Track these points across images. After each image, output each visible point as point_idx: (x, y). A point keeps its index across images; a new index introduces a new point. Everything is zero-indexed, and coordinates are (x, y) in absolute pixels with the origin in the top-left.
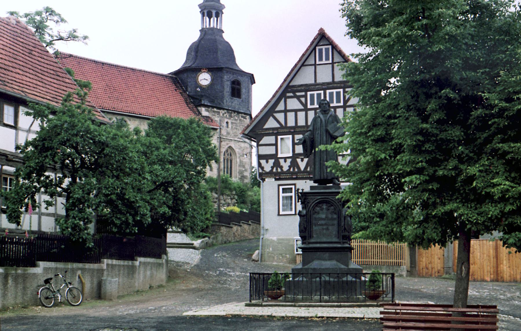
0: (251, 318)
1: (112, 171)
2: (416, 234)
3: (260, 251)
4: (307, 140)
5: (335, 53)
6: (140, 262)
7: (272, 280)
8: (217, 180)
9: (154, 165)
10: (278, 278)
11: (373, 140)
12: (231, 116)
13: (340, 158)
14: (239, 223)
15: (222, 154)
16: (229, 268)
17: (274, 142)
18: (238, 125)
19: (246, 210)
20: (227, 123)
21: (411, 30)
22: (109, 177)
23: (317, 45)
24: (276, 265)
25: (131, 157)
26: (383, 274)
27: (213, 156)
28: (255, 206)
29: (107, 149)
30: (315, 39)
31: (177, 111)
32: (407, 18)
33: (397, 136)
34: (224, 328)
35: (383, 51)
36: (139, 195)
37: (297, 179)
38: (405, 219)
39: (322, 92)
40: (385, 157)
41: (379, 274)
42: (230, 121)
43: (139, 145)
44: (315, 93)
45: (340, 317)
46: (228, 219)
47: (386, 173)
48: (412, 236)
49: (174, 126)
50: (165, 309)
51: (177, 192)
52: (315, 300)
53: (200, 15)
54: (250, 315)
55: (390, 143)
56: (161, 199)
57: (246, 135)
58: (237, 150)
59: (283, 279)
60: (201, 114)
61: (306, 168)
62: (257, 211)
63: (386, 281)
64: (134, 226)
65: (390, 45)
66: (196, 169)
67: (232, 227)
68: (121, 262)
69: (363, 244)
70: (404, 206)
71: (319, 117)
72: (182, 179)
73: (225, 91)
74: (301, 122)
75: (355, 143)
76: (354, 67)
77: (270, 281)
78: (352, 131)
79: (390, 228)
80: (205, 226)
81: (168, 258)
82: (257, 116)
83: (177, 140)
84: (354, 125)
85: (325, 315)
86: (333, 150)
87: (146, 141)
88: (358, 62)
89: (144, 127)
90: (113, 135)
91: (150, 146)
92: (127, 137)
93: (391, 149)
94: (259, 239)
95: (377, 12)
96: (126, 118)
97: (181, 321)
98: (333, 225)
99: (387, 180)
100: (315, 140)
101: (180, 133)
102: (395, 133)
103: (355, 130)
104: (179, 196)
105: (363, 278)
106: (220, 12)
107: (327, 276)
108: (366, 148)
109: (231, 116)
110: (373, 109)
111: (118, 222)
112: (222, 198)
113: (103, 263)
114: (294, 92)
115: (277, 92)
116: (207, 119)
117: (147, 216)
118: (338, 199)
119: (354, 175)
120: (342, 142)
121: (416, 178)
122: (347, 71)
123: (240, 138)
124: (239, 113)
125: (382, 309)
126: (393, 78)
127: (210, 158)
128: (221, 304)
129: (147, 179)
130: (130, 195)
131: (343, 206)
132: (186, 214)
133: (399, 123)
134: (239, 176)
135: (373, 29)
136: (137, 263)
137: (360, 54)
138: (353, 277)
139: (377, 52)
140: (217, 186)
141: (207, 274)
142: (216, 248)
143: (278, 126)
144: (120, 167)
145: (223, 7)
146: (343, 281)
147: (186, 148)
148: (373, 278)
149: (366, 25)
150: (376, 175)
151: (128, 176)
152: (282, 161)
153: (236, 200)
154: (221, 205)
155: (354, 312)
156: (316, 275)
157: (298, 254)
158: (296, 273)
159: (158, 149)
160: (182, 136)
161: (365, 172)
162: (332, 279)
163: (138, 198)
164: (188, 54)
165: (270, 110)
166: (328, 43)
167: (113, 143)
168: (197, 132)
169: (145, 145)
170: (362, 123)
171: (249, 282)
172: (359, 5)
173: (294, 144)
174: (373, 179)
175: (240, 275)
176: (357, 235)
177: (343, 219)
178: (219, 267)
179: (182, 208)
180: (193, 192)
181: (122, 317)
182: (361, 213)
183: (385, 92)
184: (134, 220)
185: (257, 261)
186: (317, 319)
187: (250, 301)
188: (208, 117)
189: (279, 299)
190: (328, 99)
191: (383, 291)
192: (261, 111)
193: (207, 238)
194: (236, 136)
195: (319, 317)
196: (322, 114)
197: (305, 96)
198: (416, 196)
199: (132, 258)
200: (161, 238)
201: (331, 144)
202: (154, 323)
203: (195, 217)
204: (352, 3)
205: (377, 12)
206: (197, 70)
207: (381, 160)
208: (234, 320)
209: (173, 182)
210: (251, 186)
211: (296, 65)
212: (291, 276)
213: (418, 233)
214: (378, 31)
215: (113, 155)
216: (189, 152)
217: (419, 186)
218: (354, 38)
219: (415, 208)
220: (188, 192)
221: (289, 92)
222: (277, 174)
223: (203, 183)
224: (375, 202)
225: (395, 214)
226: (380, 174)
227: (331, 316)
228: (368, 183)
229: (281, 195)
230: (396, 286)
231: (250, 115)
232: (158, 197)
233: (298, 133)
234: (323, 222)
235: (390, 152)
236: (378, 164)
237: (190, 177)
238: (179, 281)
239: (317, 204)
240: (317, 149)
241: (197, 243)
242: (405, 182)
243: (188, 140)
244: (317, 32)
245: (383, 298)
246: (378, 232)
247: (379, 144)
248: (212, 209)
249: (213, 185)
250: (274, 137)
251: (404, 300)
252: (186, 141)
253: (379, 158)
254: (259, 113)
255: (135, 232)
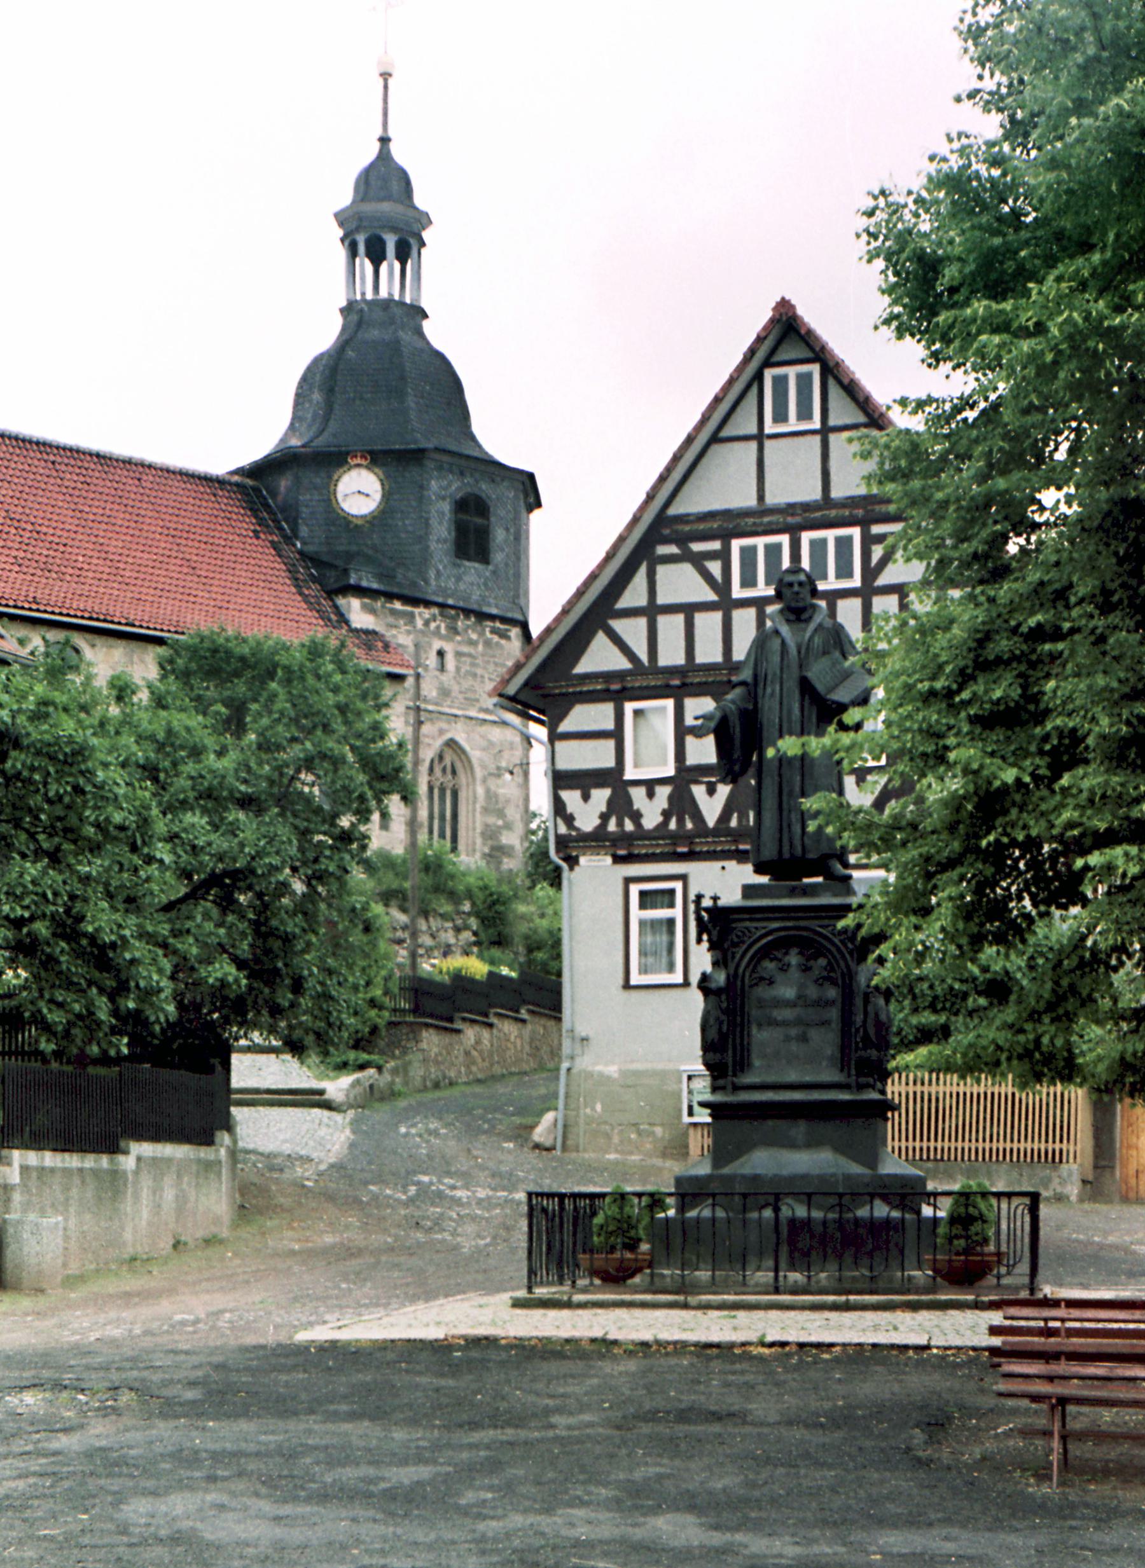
0: (534, 1347)
1: (32, 836)
2: (1122, 1059)
3: (560, 1116)
4: (731, 718)
5: (834, 391)
6: (139, 1159)
7: (607, 1217)
8: (404, 861)
9: (185, 810)
10: (627, 1209)
11: (973, 720)
12: (453, 630)
13: (849, 781)
14: (486, 1015)
15: (424, 768)
16: (449, 1174)
17: (610, 725)
18: (479, 661)
19: (511, 969)
20: (441, 654)
21: (1119, 309)
22: (24, 856)
23: (767, 363)
24: (617, 1163)
25: (104, 782)
26: (999, 1195)
27: (397, 777)
28: (540, 955)
29: (13, 754)
30: (760, 340)
31: (264, 611)
32: (1105, 263)
33: (1064, 703)
34: (443, 1382)
35: (1018, 385)
36: (132, 920)
37: (692, 856)
38: (1083, 1005)
39: (784, 539)
40: (1018, 780)
41: (985, 1195)
42: (448, 648)
43: (128, 740)
44: (760, 542)
45: (844, 1345)
46: (441, 1004)
47: (1021, 838)
48: (1106, 1063)
49: (253, 667)
50: (230, 1322)
51: (266, 906)
52: (757, 1285)
54: (530, 1339)
55: (1038, 730)
56: (211, 934)
57: (513, 699)
58: (475, 755)
59: (646, 1212)
60: (347, 622)
61: (725, 817)
62: (548, 973)
63: (1009, 1219)
64: (114, 1031)
65: (1044, 365)
66: (333, 824)
67: (458, 1031)
68: (73, 1161)
69: (926, 1089)
70: (1082, 958)
71: (777, 632)
72: (284, 862)
73: (433, 538)
74: (709, 652)
75: (907, 730)
76: (907, 447)
77: (599, 1220)
78: (897, 684)
79: (1031, 1037)
80: (367, 1030)
81: (235, 1142)
82: (548, 631)
83: (265, 721)
84: (907, 663)
85: (793, 1336)
86: (828, 754)
87: (155, 726)
88: (921, 428)
89: (144, 669)
90: (38, 704)
91: (167, 743)
92: (84, 708)
93: (1041, 753)
94: (558, 1069)
95: (997, 241)
96: (78, 640)
97: (290, 1361)
98: (825, 1023)
99: (1022, 865)
100: (761, 719)
101: (276, 695)
102: (1055, 691)
103: (911, 681)
104: (274, 923)
105: (927, 1211)
106: (412, 241)
107: (801, 1202)
108: (947, 748)
109: (453, 630)
110: (977, 605)
111: (56, 1017)
112: (424, 927)
113: (9, 1164)
114: (682, 540)
115: (621, 539)
116: (368, 638)
117: (163, 996)
118: (845, 930)
119: (904, 844)
120: (858, 727)
121: (1126, 854)
122: (882, 463)
123: (486, 711)
124: (482, 616)
125: (996, 1318)
126: (1052, 489)
127: (384, 786)
128: (427, 1300)
129: (161, 861)
130: (102, 919)
131: (862, 958)
132: (298, 986)
133: (1073, 652)
134: (482, 847)
135: (980, 307)
136: (128, 1162)
137: (930, 400)
138: (894, 1207)
139: (995, 389)
140: (407, 885)
141: (375, 1197)
142: (402, 1103)
143: (624, 664)
144: (60, 819)
145: (424, 221)
146: (857, 1220)
147: (297, 747)
148: (962, 1210)
149: (953, 290)
150: (984, 843)
151: (91, 851)
152: (638, 794)
153: (475, 934)
154: (421, 951)
155: (896, 1328)
156: (762, 1200)
157: (695, 1125)
158: (690, 1192)
159: (196, 752)
160: (282, 703)
161: (944, 836)
162: (817, 1214)
163: (127, 932)
164: (301, 398)
165: (596, 610)
166: (811, 355)
167: (37, 733)
168: (336, 690)
169: (152, 738)
170: (937, 655)
171: (524, 1224)
172: (927, 211)
173: (681, 732)
174: (970, 858)
175: (489, 1198)
176: (909, 1058)
177: (859, 1002)
178: (415, 1173)
179: (286, 965)
180: (323, 906)
181: (80, 1350)
182: (920, 979)
183: (1022, 541)
184: (115, 1013)
185: (548, 1149)
186: (766, 1351)
187: (530, 1289)
188: (374, 633)
189: (629, 1282)
190: (805, 564)
191: (999, 1254)
192: (565, 612)
193: (372, 1071)
194: (472, 701)
195: (772, 1345)
196: (788, 621)
197: (724, 556)
198: (1129, 918)
199: (112, 1147)
200: (210, 1070)
201: (820, 733)
202: (195, 1367)
203: (331, 998)
204: (905, 206)
205: (997, 241)
206: (330, 461)
207: (1005, 789)
208: (475, 1354)
209: (253, 872)
210: (528, 883)
211: (689, 440)
212: (670, 1201)
213: (1130, 1049)
214: (1001, 311)
215: (37, 777)
216: (308, 764)
217: (1137, 884)
218: (908, 338)
219: (1122, 964)
220: (305, 908)
221: (666, 541)
222: (624, 838)
223: (358, 875)
224: (977, 941)
225: (1049, 985)
226: (997, 841)
227: (813, 1339)
228: (954, 874)
229: (636, 914)
230: (1042, 1233)
231: (524, 626)
232: (199, 926)
233: (699, 690)
234: (787, 1014)
235: (1037, 761)
236: (988, 804)
237: (311, 855)
238: (276, 1222)
239: (766, 953)
240: (770, 753)
241: (338, 1087)
242: (1087, 868)
243: (308, 720)
244: (769, 314)
245: (999, 1277)
246: (984, 1048)
247: (999, 734)
248: (390, 965)
249: (390, 881)
251: (1071, 1286)
252: (295, 721)
253: (997, 783)
254: (558, 620)
255: (119, 1051)
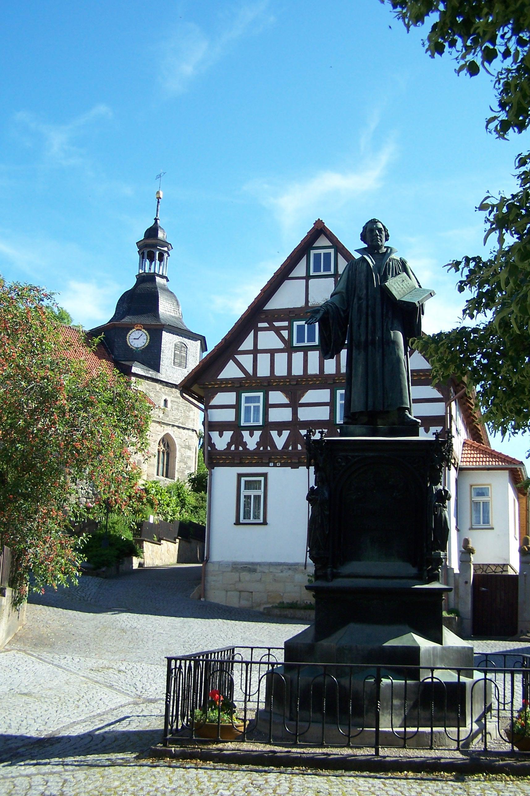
17: (234, 402)
20: (166, 401)
53: (137, 257)
61: (286, 446)
74: (281, 371)
197: (290, 329)
250: (234, 394)
